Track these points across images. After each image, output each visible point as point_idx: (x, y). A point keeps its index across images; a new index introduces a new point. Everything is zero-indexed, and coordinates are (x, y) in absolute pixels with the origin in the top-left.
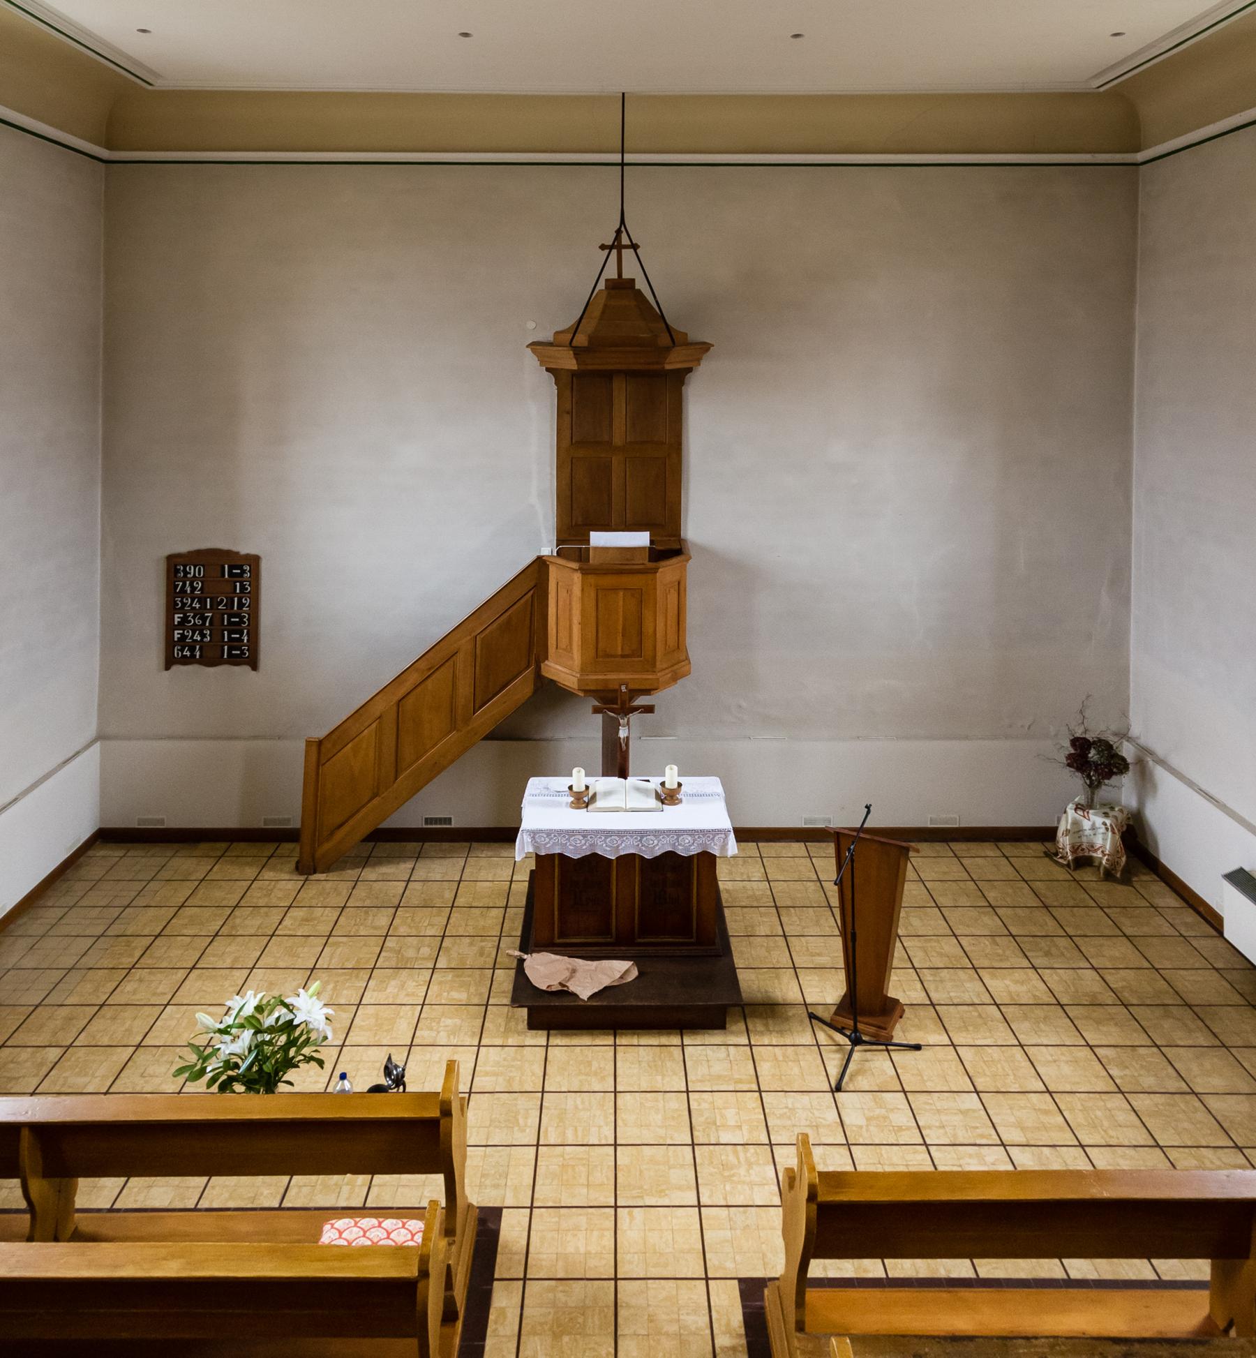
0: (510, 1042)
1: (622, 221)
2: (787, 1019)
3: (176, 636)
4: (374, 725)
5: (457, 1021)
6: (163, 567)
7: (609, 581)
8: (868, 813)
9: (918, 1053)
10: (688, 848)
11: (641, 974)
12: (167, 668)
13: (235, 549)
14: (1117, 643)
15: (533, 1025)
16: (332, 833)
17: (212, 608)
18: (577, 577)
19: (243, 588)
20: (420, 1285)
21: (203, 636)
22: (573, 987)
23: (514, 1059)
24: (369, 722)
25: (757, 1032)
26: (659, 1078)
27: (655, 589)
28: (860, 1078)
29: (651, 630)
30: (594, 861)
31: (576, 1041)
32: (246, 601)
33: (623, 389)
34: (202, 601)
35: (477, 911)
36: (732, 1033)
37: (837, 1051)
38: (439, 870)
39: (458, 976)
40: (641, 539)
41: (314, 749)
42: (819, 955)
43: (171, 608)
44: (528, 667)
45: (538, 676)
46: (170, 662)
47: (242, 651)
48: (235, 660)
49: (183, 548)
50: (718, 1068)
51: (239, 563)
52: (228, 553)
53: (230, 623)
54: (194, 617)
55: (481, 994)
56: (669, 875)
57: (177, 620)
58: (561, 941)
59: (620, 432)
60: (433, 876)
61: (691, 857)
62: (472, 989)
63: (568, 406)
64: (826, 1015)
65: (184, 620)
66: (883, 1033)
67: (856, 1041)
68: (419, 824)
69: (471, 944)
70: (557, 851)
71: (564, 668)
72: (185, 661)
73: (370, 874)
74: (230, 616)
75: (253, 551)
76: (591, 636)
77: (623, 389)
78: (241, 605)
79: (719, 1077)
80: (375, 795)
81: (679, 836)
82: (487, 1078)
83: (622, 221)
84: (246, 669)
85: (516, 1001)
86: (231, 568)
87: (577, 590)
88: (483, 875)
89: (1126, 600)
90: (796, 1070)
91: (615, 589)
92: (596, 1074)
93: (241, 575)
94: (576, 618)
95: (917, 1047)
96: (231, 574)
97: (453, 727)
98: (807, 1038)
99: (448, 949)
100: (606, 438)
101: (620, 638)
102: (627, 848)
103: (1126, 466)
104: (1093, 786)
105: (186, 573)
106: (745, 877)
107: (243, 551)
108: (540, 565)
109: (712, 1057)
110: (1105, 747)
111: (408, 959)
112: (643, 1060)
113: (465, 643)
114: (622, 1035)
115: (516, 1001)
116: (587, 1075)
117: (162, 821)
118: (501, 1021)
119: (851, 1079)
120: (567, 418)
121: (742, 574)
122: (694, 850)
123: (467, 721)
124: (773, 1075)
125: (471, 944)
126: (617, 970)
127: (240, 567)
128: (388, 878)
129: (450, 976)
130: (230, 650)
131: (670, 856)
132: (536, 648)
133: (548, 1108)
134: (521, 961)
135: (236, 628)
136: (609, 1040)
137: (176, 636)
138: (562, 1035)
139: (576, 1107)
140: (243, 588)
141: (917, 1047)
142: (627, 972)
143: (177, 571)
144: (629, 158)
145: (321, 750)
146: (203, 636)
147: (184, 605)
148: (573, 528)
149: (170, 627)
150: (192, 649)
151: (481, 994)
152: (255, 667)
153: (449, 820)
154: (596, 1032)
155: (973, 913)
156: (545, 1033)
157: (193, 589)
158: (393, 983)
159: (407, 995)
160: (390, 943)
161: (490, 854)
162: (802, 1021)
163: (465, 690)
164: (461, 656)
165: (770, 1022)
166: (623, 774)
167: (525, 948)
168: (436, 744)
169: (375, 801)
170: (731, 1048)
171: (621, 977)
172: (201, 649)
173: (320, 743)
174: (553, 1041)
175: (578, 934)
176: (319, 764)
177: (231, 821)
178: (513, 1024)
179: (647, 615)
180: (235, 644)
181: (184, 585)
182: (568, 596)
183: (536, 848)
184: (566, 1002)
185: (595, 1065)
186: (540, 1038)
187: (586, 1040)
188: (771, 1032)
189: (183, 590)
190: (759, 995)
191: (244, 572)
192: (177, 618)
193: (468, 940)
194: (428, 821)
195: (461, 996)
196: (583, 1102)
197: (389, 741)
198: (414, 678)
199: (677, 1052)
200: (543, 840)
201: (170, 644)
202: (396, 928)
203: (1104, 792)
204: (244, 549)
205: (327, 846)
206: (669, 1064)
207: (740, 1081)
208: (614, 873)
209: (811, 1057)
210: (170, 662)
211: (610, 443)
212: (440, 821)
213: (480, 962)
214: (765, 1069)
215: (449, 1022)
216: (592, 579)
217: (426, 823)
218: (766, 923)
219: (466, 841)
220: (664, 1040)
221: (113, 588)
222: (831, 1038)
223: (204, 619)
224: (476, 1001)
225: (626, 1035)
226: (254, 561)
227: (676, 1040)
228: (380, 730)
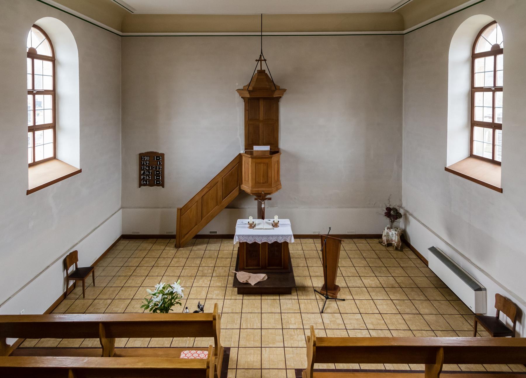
0: (233, 298)
1: (262, 53)
6: (138, 157)
7: (259, 161)
10: (281, 240)
11: (268, 278)
12: (140, 187)
13: (158, 151)
14: (399, 178)
17: (151, 170)
19: (160, 163)
20: (207, 370)
21: (149, 177)
22: (250, 282)
30: (255, 244)
33: (263, 101)
34: (149, 167)
41: (179, 211)
43: (141, 169)
46: (140, 185)
48: (158, 185)
49: (143, 151)
50: (289, 306)
52: (156, 153)
59: (262, 116)
65: (144, 173)
66: (334, 295)
67: (327, 298)
70: (245, 241)
71: (247, 187)
72: (145, 185)
76: (254, 177)
77: (263, 101)
78: (159, 168)
79: (290, 309)
80: (196, 225)
83: (262, 53)
84: (161, 187)
86: (157, 157)
87: (250, 163)
89: (400, 166)
90: (311, 307)
91: (260, 163)
93: (159, 159)
94: (250, 172)
97: (217, 205)
102: (264, 240)
103: (401, 125)
104: (392, 222)
107: (160, 152)
108: (240, 156)
109: (288, 302)
110: (395, 210)
112: (269, 303)
118: (230, 292)
120: (247, 112)
121: (295, 158)
122: (282, 241)
127: (159, 157)
128: (200, 249)
129: (216, 278)
131: (276, 243)
132: (239, 181)
134: (236, 274)
136: (260, 298)
140: (160, 163)
141: (344, 300)
144: (263, 34)
145: (181, 211)
146: (149, 177)
148: (249, 146)
149: (140, 175)
150: (146, 181)
152: (163, 187)
158: (201, 280)
163: (220, 193)
164: (219, 184)
173: (181, 209)
176: (181, 215)
177: (157, 232)
182: (248, 164)
184: (248, 286)
185: (256, 305)
186: (240, 297)
189: (144, 164)
192: (142, 172)
194: (210, 232)
195: (219, 284)
198: (206, 190)
199: (278, 301)
200: (241, 238)
201: (140, 180)
203: (395, 224)
204: (160, 152)
205: (183, 240)
207: (295, 310)
210: (140, 185)
214: (302, 306)
215: (216, 292)
216: (254, 160)
218: (302, 263)
220: (274, 297)
221: (125, 164)
223: (149, 172)
224: (223, 286)
226: (163, 155)
228: (197, 206)
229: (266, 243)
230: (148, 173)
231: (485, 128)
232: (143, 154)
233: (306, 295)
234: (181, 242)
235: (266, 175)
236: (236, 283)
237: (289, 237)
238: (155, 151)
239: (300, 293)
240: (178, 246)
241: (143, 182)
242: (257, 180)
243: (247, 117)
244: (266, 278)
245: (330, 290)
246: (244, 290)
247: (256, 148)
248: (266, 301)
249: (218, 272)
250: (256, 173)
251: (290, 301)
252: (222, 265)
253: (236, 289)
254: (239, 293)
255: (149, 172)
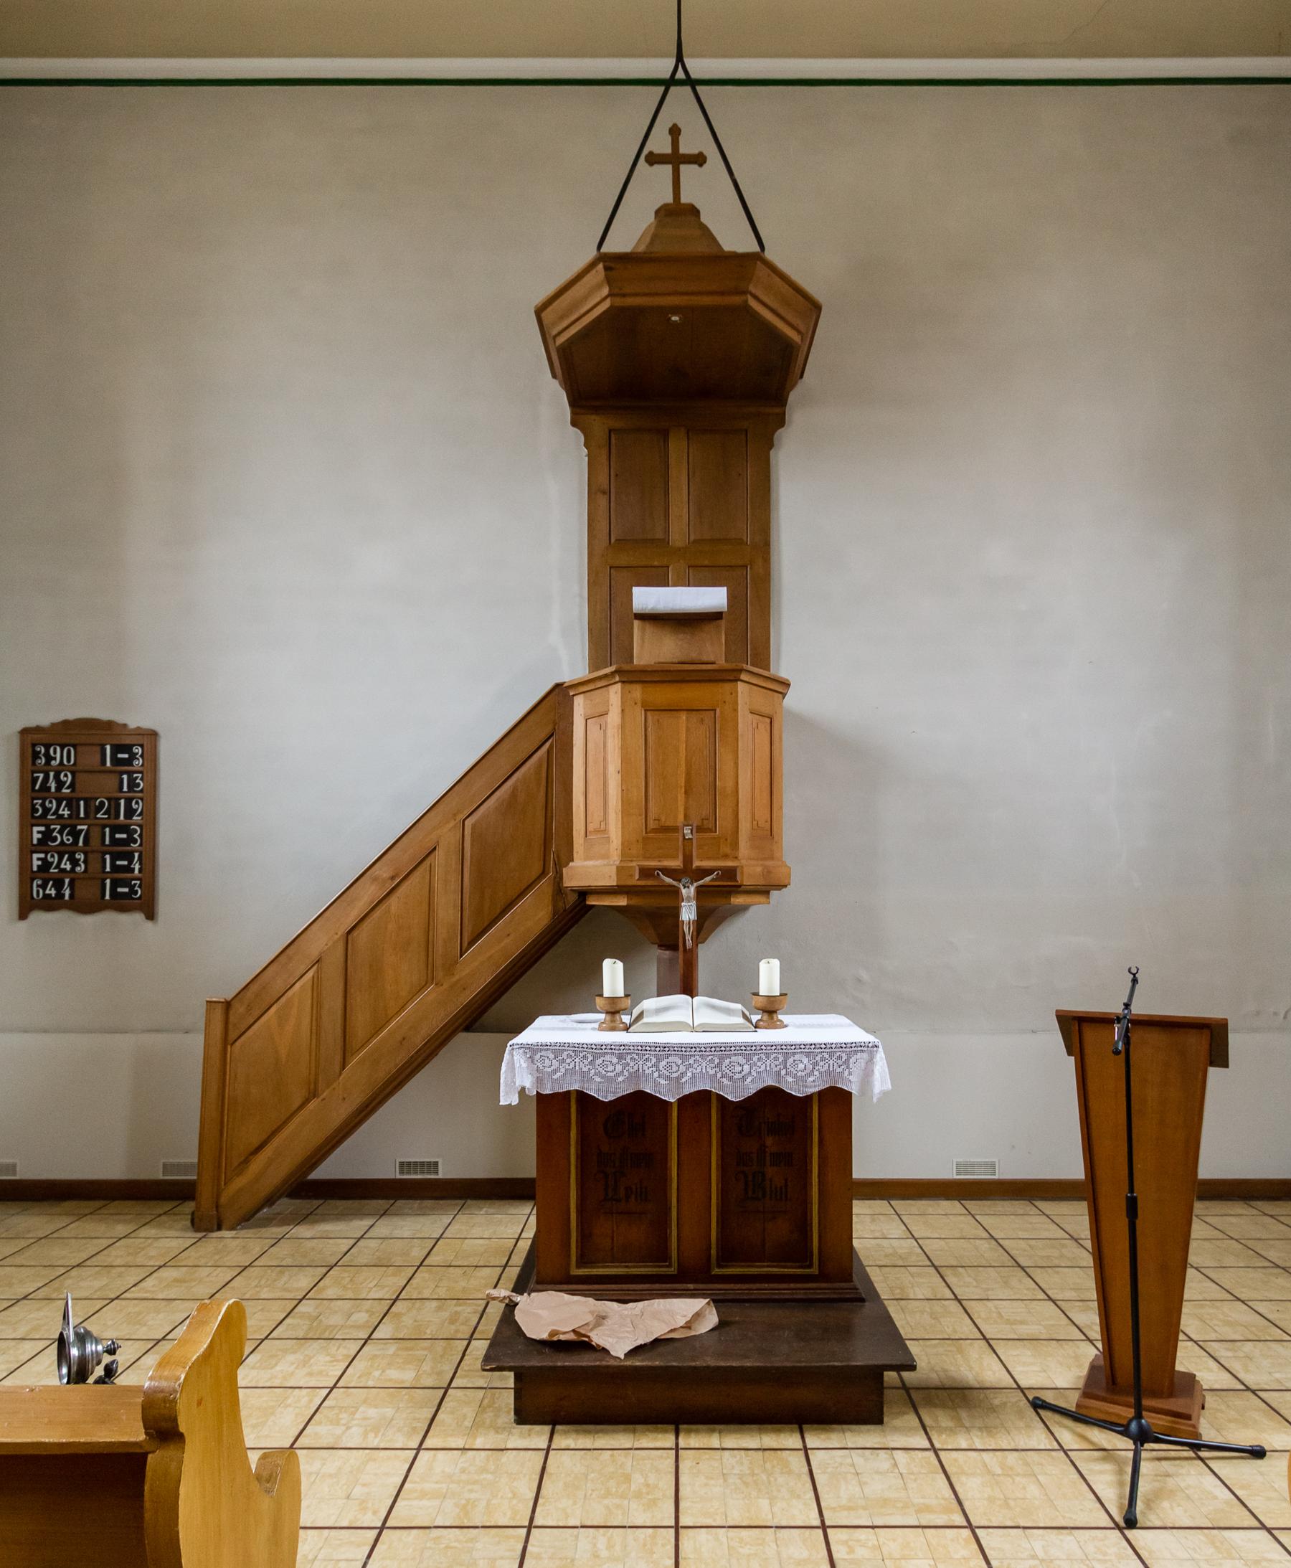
0: (479, 1443)
2: (993, 1409)
3: (36, 863)
4: (311, 974)
5: (389, 1412)
7: (664, 694)
8: (1135, 981)
9: (1259, 1462)
10: (803, 1081)
11: (722, 1325)
12: (23, 915)
13: (119, 719)
15: (524, 1416)
16: (246, 1161)
18: (615, 694)
19: (132, 785)
21: (75, 863)
22: (597, 1338)
23: (484, 1470)
24: (302, 969)
25: (941, 1430)
26: (764, 1503)
27: (736, 710)
28: (1166, 1504)
29: (730, 784)
30: (639, 1108)
31: (603, 1441)
32: (138, 806)
33: (682, 385)
34: (72, 803)
35: (459, 1271)
36: (896, 1429)
37: (1104, 1459)
38: (410, 1229)
39: (407, 1349)
40: (713, 598)
41: (218, 1014)
42: (1022, 1323)
43: (29, 816)
44: (544, 873)
45: (559, 890)
46: (26, 907)
47: (132, 887)
48: (122, 903)
49: (45, 720)
50: (876, 1487)
51: (127, 741)
52: (109, 725)
53: (114, 842)
54: (61, 832)
55: (439, 1374)
56: (769, 1141)
57: (36, 836)
58: (581, 1272)
60: (397, 1233)
61: (809, 1098)
62: (426, 1367)
63: (603, 479)
64: (1070, 1402)
65: (47, 836)
66: (1183, 1425)
67: (1143, 1437)
68: (387, 1171)
69: (439, 1309)
71: (596, 863)
72: (50, 904)
73: (303, 1231)
74: (115, 829)
75: (146, 723)
77: (682, 385)
78: (130, 812)
79: (885, 1502)
80: (314, 1094)
81: (787, 1056)
82: (425, 1503)
84: (138, 917)
85: (492, 1362)
86: (117, 748)
87: (614, 717)
88: (476, 1232)
90: (1033, 1490)
91: (672, 710)
92: (638, 1495)
93: (129, 762)
94: (614, 765)
95: (1258, 1453)
96: (116, 762)
97: (430, 978)
98: (1039, 1438)
99: (398, 1315)
100: (659, 535)
101: (681, 797)
102: (695, 1079)
105: (49, 759)
106: (877, 1235)
107: (132, 724)
109: (862, 1469)
111: (328, 1327)
112: (729, 1473)
113: (447, 836)
114: (689, 1432)
115: (492, 1362)
116: (623, 1497)
117: (13, 1168)
118: (470, 1412)
119: (1148, 1504)
120: (602, 501)
121: (861, 760)
123: (450, 968)
124: (991, 1500)
125: (439, 1309)
126: (680, 1314)
127: (128, 748)
128: (333, 1234)
129: (392, 1348)
130: (115, 884)
131: (771, 1096)
133: (538, 1557)
134: (511, 1306)
135: (121, 851)
136: (667, 1440)
137: (36, 863)
138: (577, 1432)
139: (596, 1556)
140: (132, 785)
141: (1258, 1453)
142: (698, 1316)
143: (36, 755)
145: (230, 1017)
147: (46, 811)
148: (610, 627)
149: (26, 849)
150: (59, 885)
151: (439, 1374)
152: (151, 915)
153: (434, 1167)
154: (639, 1427)
155: (1258, 1275)
156: (547, 1428)
157: (60, 785)
158: (291, 1358)
159: (310, 1374)
160: (305, 1307)
161: (491, 1211)
162: (1020, 1414)
163: (447, 913)
164: (439, 857)
165: (963, 1414)
166: (688, 988)
167: (520, 1287)
168: (403, 1008)
169: (312, 1105)
170: (898, 1454)
171: (688, 1326)
172: (72, 885)
173: (228, 1005)
174: (561, 1441)
175: (614, 1260)
176: (226, 1042)
177: (112, 1169)
178: (489, 1416)
179: (723, 754)
180: (121, 876)
181: (46, 779)
182: (602, 744)
183: (539, 1081)
184: (585, 1360)
185: (638, 1480)
186: (537, 1436)
187: (622, 1439)
188: (968, 1430)
189: (45, 787)
190: (934, 1376)
191: (133, 756)
193: (434, 1304)
194: (404, 1167)
195: (408, 1376)
196: (610, 1547)
197: (333, 1002)
198: (368, 893)
199: (797, 1460)
200: (550, 1064)
201: (26, 876)
202: (323, 1289)
204: (135, 720)
205: (239, 1182)
206: (781, 1480)
207: (927, 1509)
208: (674, 1233)
209: (1056, 1468)
210: (26, 907)
211: (664, 542)
212: (422, 1166)
213: (449, 1331)
214: (971, 1488)
215: (372, 1412)
216: (637, 691)
217: (402, 1172)
218: (926, 1284)
219: (460, 1198)
220: (769, 1440)
222: (1084, 1438)
223: (75, 834)
224: (429, 1382)
225: (697, 1431)
227: (792, 1440)
228: (317, 984)
229: (704, 1096)
230: (68, 840)
231: (1186, 1296)
232: (38, 729)
233: (987, 1429)
234: (223, 1200)
235: (706, 783)
236: (508, 1343)
237: (859, 1060)
238: (103, 715)
239: (939, 1418)
240: (208, 1222)
241: (42, 892)
242: (652, 815)
243: (603, 525)
244: (712, 1319)
245: (1139, 1393)
246: (563, 1392)
247: (647, 598)
248: (709, 1462)
249: (407, 1321)
250: (646, 770)
251: (883, 1459)
252: (442, 1293)
253: (509, 1379)
254: (526, 1413)
255: (75, 834)
